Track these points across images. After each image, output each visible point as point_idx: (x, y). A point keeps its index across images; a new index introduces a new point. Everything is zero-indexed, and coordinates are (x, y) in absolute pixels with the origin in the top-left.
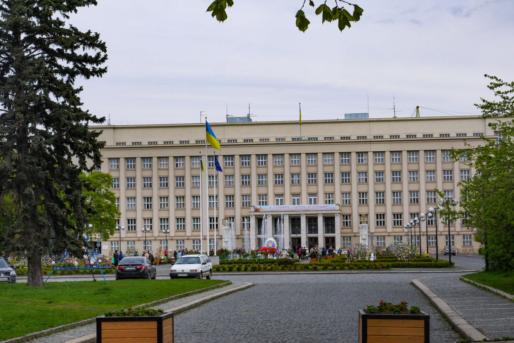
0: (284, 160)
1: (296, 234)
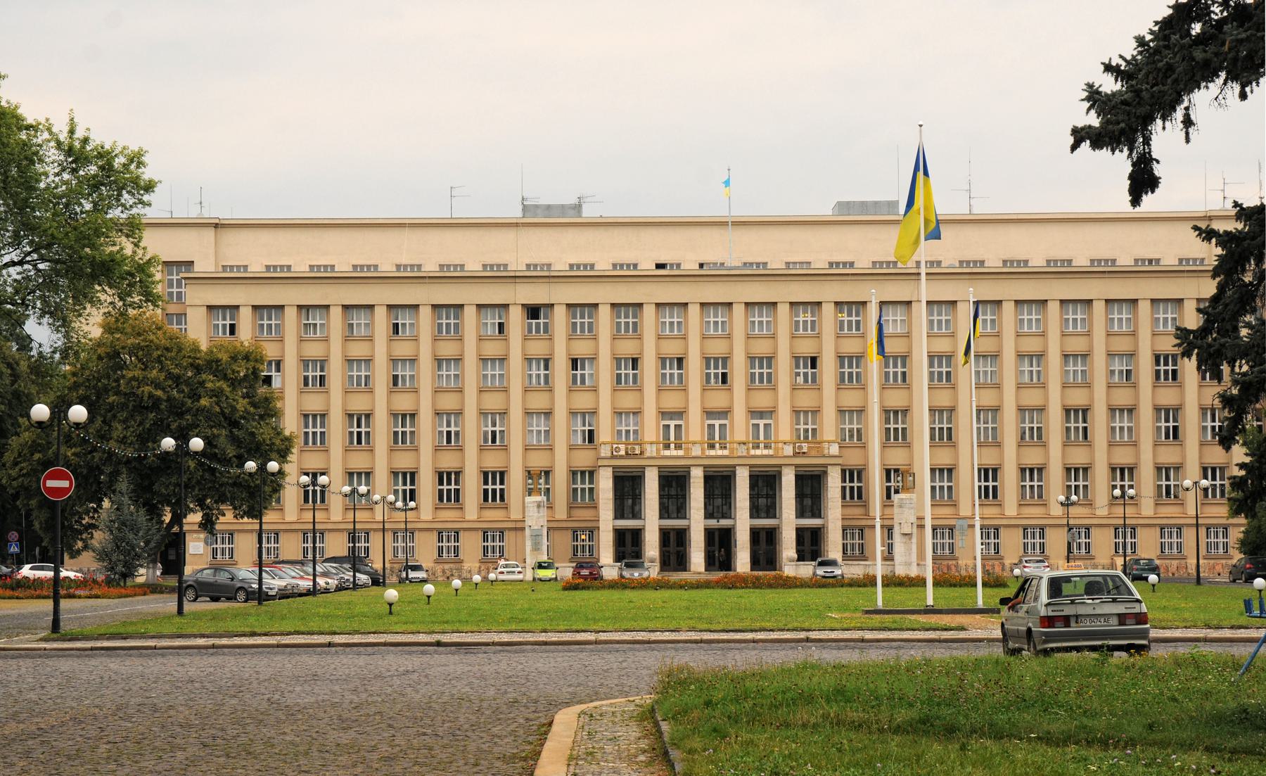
0: (283, 321)
1: (718, 519)
